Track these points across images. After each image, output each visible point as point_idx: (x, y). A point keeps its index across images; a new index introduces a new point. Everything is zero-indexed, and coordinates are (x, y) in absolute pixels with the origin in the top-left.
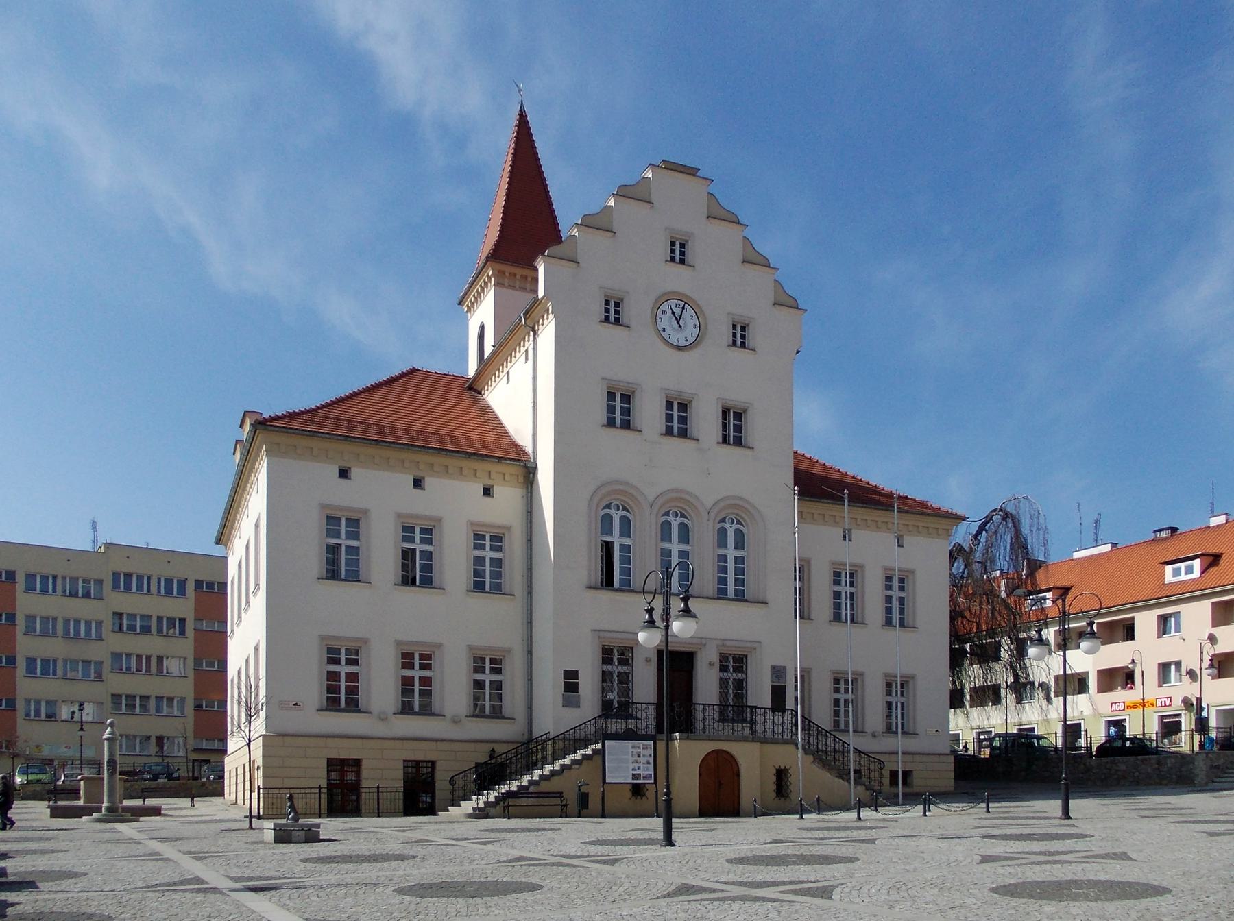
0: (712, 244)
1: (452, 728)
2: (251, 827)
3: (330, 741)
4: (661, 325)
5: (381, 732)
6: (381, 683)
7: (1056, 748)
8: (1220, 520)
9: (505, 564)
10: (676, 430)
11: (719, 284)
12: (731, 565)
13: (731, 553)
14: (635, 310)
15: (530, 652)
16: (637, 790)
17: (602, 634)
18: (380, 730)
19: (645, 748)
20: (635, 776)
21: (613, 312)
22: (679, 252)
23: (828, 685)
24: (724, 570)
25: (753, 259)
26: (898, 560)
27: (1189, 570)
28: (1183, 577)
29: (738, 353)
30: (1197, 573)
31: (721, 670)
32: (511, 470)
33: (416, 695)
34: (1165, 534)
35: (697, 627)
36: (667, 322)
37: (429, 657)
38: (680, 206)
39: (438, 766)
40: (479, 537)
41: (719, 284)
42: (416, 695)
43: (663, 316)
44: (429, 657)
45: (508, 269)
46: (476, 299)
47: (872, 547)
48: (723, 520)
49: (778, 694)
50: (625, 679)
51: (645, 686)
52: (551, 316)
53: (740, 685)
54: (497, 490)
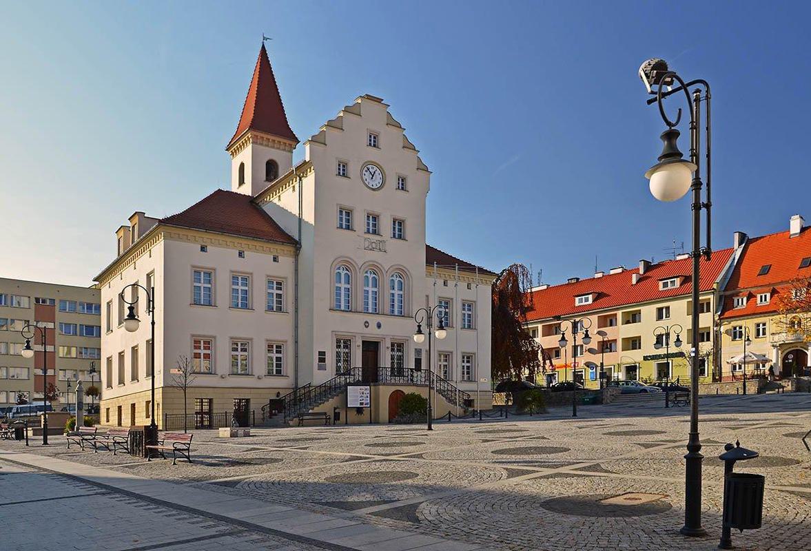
0: (388, 137)
1: (261, 385)
2: (27, 445)
3: (235, 390)
4: (364, 177)
5: (224, 384)
6: (260, 360)
7: (568, 383)
8: (600, 275)
9: (284, 297)
10: (344, 227)
11: (391, 158)
12: (396, 298)
13: (343, 286)
14: (353, 170)
15: (296, 342)
16: (359, 410)
17: (337, 333)
18: (222, 383)
19: (366, 389)
20: (361, 404)
21: (343, 170)
22: (374, 141)
23: (264, 347)
24: (339, 295)
25: (409, 146)
26: (469, 295)
27: (587, 300)
28: (584, 303)
29: (401, 193)
30: (590, 301)
31: (337, 348)
32: (289, 249)
33: (241, 368)
34: (573, 281)
35: (389, 329)
36: (367, 176)
37: (280, 347)
38: (373, 119)
39: (252, 401)
40: (235, 278)
41: (391, 158)
42: (241, 368)
43: (366, 173)
44: (280, 347)
45: (260, 134)
46: (241, 146)
47: (458, 289)
48: (393, 276)
49: (418, 362)
50: (348, 355)
51: (357, 361)
52: (313, 171)
53: (400, 358)
54: (280, 258)
